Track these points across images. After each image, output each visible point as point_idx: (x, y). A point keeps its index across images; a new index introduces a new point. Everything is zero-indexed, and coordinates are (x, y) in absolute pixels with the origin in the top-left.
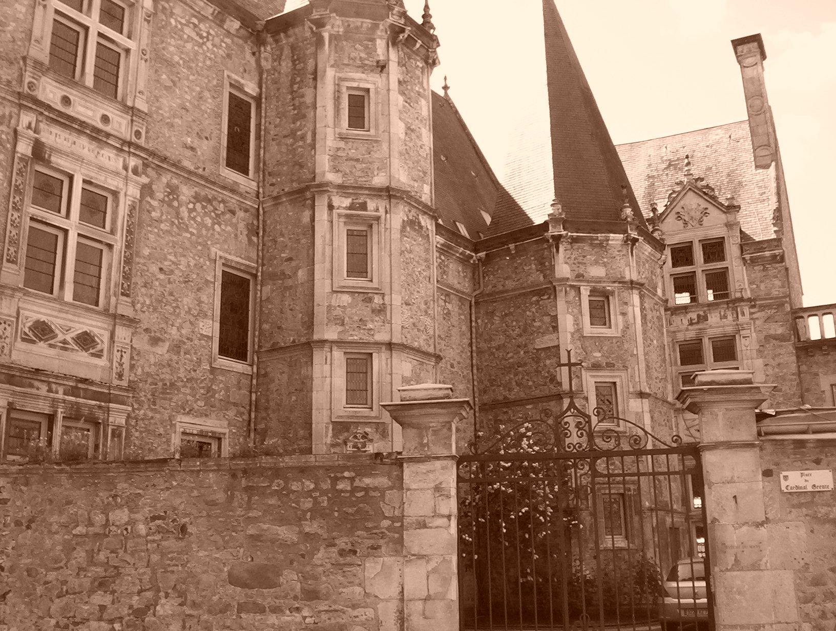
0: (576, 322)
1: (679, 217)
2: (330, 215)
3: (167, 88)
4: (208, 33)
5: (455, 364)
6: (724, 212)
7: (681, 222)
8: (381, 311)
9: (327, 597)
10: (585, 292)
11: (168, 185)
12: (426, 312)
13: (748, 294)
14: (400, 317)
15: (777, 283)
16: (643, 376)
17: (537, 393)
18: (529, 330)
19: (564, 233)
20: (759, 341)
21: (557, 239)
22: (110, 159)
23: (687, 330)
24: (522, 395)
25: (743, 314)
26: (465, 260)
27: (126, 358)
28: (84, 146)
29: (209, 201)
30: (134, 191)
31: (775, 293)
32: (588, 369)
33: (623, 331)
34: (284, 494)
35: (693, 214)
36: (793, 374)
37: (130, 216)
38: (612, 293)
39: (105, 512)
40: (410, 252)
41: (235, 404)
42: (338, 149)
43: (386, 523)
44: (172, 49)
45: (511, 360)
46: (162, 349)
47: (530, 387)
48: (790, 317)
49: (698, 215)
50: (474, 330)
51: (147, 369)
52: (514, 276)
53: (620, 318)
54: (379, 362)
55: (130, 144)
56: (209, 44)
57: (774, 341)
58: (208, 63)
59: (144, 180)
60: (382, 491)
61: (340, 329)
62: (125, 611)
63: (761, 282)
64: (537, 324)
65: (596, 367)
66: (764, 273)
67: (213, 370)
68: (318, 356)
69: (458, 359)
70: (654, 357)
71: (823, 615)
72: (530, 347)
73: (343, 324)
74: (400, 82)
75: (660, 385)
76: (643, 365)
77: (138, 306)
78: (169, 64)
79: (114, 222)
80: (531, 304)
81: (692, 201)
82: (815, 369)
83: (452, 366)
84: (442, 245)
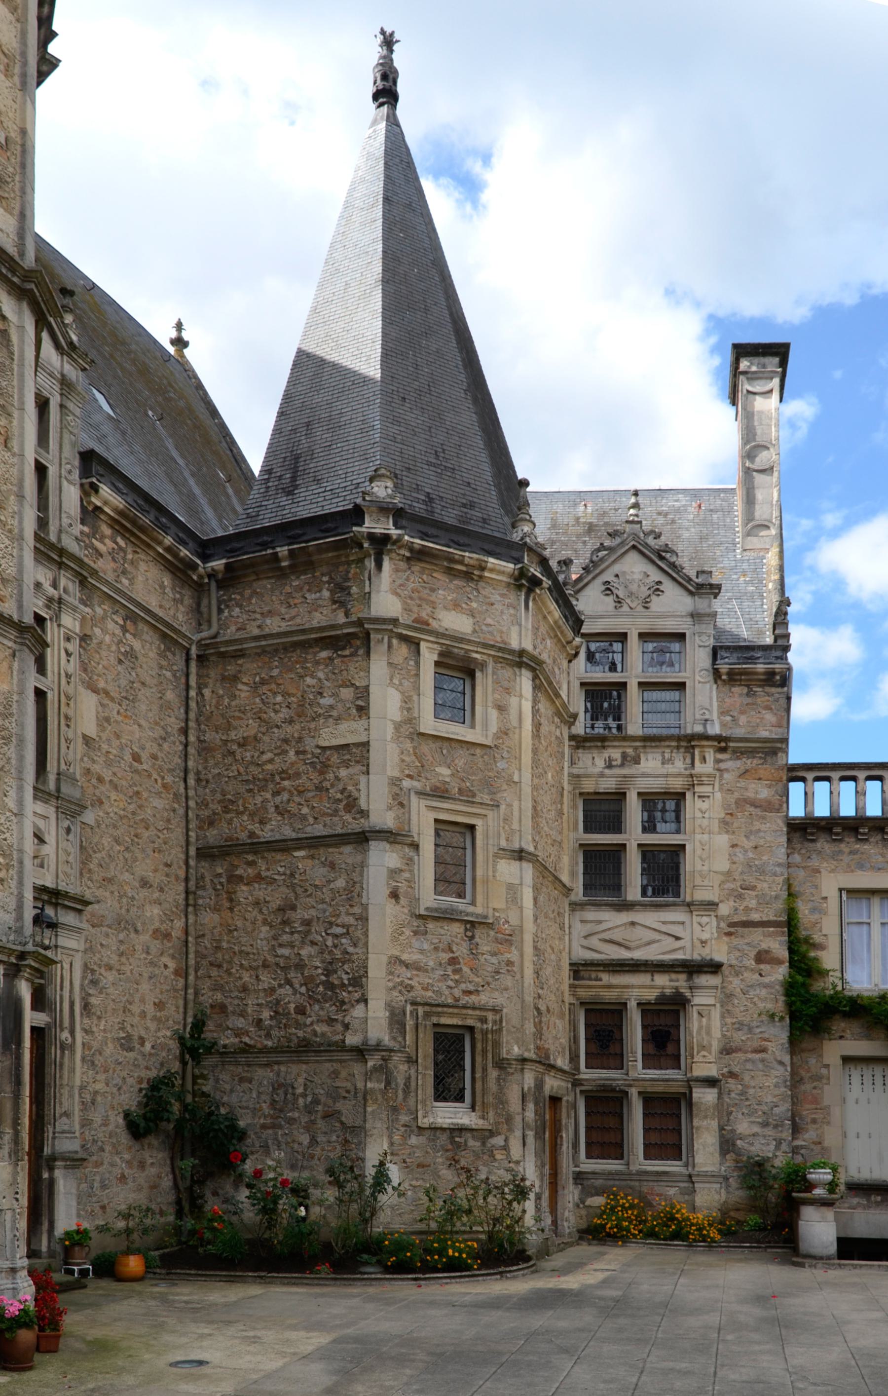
0: (407, 704)
1: (608, 590)
5: (144, 756)
6: (691, 593)
7: (610, 600)
10: (429, 656)
13: (715, 729)
15: (769, 717)
16: (528, 823)
17: (319, 830)
18: (310, 712)
19: (394, 532)
20: (725, 806)
21: (381, 542)
23: (602, 775)
24: (288, 833)
25: (704, 760)
26: (180, 570)
31: (764, 734)
32: (421, 794)
33: (497, 737)
35: (634, 588)
36: (779, 865)
38: (483, 666)
45: (269, 767)
47: (304, 818)
49: (644, 592)
50: (193, 705)
52: (283, 610)
53: (494, 714)
57: (752, 809)
63: (742, 712)
64: (326, 701)
65: (439, 793)
66: (749, 700)
70: (546, 799)
75: (550, 849)
76: (528, 805)
80: (317, 663)
81: (634, 568)
82: (815, 862)
83: (136, 758)
84: (121, 513)
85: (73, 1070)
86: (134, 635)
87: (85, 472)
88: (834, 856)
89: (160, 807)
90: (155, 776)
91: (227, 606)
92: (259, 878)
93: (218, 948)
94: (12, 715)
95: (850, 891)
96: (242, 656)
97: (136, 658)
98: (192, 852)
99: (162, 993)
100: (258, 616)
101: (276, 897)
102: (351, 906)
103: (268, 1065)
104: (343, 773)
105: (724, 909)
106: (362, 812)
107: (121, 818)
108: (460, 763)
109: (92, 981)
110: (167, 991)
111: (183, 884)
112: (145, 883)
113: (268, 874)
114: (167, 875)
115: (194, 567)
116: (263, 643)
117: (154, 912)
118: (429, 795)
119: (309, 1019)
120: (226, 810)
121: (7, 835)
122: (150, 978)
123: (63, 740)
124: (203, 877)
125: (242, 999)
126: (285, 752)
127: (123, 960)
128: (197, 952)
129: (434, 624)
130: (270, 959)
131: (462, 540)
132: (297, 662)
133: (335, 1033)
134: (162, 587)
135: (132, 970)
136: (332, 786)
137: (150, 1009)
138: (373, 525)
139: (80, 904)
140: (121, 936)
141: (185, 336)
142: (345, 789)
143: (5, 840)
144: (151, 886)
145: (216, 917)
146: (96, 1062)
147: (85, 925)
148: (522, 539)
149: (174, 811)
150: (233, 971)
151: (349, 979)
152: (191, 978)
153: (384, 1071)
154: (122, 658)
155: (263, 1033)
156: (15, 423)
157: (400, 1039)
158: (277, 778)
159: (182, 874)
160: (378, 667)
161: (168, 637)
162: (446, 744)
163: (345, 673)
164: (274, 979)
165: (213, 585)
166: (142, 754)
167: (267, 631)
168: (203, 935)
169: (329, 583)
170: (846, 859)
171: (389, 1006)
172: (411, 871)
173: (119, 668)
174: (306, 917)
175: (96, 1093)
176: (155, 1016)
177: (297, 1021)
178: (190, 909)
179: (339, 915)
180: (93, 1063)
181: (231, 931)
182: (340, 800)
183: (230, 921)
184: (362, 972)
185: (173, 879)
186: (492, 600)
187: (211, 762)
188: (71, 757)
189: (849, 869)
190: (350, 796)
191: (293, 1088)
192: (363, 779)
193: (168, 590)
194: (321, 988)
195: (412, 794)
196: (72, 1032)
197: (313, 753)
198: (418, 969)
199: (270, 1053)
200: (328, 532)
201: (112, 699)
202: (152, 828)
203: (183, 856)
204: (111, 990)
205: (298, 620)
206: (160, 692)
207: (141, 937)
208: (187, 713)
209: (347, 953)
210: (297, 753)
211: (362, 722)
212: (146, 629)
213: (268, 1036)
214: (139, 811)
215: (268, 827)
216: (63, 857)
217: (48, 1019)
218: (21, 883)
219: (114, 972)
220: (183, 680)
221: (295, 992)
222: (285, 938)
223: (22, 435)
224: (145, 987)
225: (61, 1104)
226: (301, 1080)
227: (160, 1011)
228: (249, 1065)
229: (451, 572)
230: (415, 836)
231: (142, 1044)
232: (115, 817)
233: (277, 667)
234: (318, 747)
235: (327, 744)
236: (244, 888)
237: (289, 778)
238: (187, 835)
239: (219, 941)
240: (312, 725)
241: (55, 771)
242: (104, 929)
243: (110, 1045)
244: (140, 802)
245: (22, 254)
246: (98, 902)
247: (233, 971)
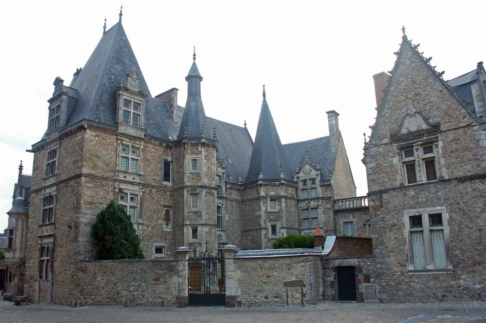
0: (266, 208)
2: (188, 193)
3: (148, 166)
4: (158, 149)
5: (234, 220)
8: (200, 216)
9: (167, 283)
10: (269, 199)
11: (149, 190)
12: (213, 214)
13: (321, 196)
14: (205, 217)
17: (256, 228)
20: (323, 210)
21: (261, 185)
22: (136, 188)
23: (305, 206)
25: (320, 202)
26: (238, 190)
27: (141, 232)
28: (130, 187)
29: (160, 191)
30: (141, 194)
31: (329, 195)
32: (268, 221)
34: (161, 265)
35: (307, 171)
37: (141, 200)
39: (133, 268)
40: (208, 200)
41: (168, 239)
43: (176, 271)
44: (149, 156)
46: (150, 229)
47: (254, 226)
48: (333, 203)
49: (309, 171)
51: (146, 234)
54: (199, 229)
55: (139, 183)
56: (158, 152)
58: (158, 156)
59: (144, 190)
60: (176, 265)
61: (190, 221)
62: (137, 285)
63: (325, 192)
64: (256, 208)
65: (271, 220)
67: (162, 232)
68: (185, 228)
69: (235, 218)
71: (242, 287)
73: (191, 220)
74: (205, 156)
77: (144, 220)
78: (148, 160)
79: (137, 202)
83: (233, 221)
88: (342, 216)
95: (344, 223)
101: (252, 238)
104: (258, 219)
105: (324, 228)
138: (260, 182)
170: (344, 217)
189: (344, 219)
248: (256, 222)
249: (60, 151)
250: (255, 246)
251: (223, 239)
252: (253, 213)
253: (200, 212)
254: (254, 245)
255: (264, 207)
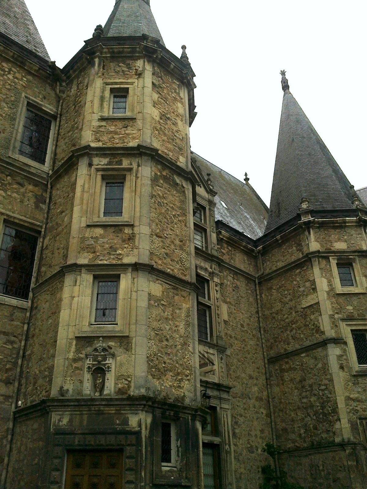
5: (245, 324)
8: (131, 238)
10: (334, 262)
17: (308, 343)
18: (297, 295)
21: (308, 225)
24: (298, 347)
26: (249, 253)
32: (343, 320)
38: (354, 260)
42: (100, 127)
45: (287, 320)
50: (259, 301)
52: (282, 258)
61: (91, 256)
64: (302, 289)
72: (299, 308)
73: (94, 252)
80: (296, 275)
83: (242, 326)
84: (228, 238)
85: (231, 463)
86: (237, 280)
87: (217, 228)
89: (252, 344)
90: (249, 332)
91: (265, 262)
92: (291, 369)
93: (281, 402)
94: (190, 316)
96: (272, 279)
97: (239, 288)
98: (266, 362)
99: (262, 425)
100: (275, 263)
101: (297, 376)
102: (326, 375)
103: (306, 456)
104: (312, 317)
106: (322, 332)
107: (240, 351)
108: (355, 303)
109: (235, 422)
110: (264, 424)
111: (265, 376)
112: (251, 377)
113: (293, 366)
114: (258, 373)
115: (253, 251)
116: (278, 272)
117: (255, 389)
118: (346, 319)
119: (319, 432)
120: (276, 341)
121: (190, 361)
122: (257, 419)
123: (217, 323)
124: (272, 372)
125: (293, 425)
126: (291, 313)
127: (246, 411)
128: (273, 405)
129: (333, 249)
130: (300, 404)
131: (335, 214)
132: (290, 277)
133: (330, 437)
134: (244, 260)
135: (250, 416)
136: (310, 323)
137: (258, 433)
138: (304, 219)
139: (226, 389)
140: (244, 401)
141: (248, 177)
142: (314, 324)
143: (189, 363)
144: (253, 378)
145: (278, 388)
146: (240, 459)
147: (230, 398)
148: (357, 207)
149: (258, 345)
150: (288, 412)
151: (331, 410)
152: (273, 417)
153: (354, 455)
154: (234, 289)
155: (302, 440)
156: (188, 218)
157: (358, 437)
158: (290, 325)
159: (264, 371)
160: (316, 271)
161: (248, 278)
162: (348, 296)
163: (306, 276)
164: (303, 414)
165: (260, 255)
166: (244, 324)
167: (278, 267)
168: (275, 397)
169: (294, 244)
171: (349, 421)
172: (346, 355)
173: (234, 293)
174: (310, 383)
175: (241, 473)
176: (261, 436)
177: (314, 433)
178: (269, 386)
179: (322, 381)
180: (239, 460)
181: (284, 394)
182: (314, 329)
183: (283, 390)
184: (335, 406)
185: (260, 374)
186: (351, 234)
187: (268, 323)
188: (220, 329)
190: (317, 326)
191: (318, 467)
192: (320, 318)
193: (246, 261)
194: (321, 416)
195: (339, 320)
196: (230, 446)
197: (301, 311)
198: (359, 401)
199: (306, 450)
200: (292, 225)
201: (232, 305)
202: (251, 353)
203: (263, 364)
204: (243, 426)
205: (287, 261)
206: (248, 299)
207: (252, 401)
208: (257, 305)
209: (328, 398)
210: (295, 312)
211: (315, 294)
212: (240, 277)
213: (305, 442)
214: (245, 347)
215: (291, 346)
216: (220, 370)
217: (220, 440)
218: (195, 380)
219: (243, 417)
220: (255, 293)
221: (312, 419)
222: (304, 394)
223: (189, 221)
224: (256, 423)
225: (228, 479)
226: (321, 463)
227: (263, 434)
228: (300, 457)
229: (335, 228)
230: (344, 339)
231: (257, 450)
232: (237, 351)
233: (283, 280)
234: (302, 308)
235: (305, 306)
236: (286, 374)
237: (294, 324)
238: (264, 354)
239: (280, 399)
240: (299, 300)
241: (216, 336)
242: (238, 399)
243: (244, 451)
244: (245, 343)
245: (187, 168)
246: (234, 387)
247: (288, 412)
248: (306, 325)
249: (102, 405)
250: (313, 399)
251: (217, 372)
252: (292, 304)
253: (132, 226)
254: (306, 397)
255: (325, 281)
